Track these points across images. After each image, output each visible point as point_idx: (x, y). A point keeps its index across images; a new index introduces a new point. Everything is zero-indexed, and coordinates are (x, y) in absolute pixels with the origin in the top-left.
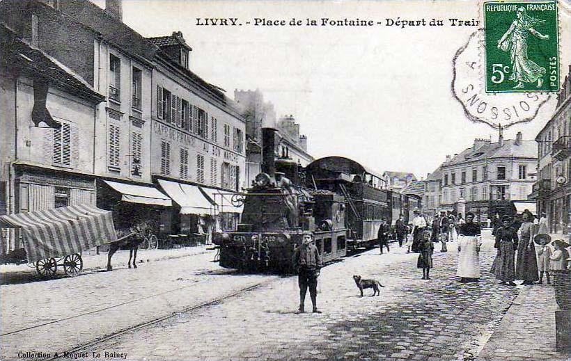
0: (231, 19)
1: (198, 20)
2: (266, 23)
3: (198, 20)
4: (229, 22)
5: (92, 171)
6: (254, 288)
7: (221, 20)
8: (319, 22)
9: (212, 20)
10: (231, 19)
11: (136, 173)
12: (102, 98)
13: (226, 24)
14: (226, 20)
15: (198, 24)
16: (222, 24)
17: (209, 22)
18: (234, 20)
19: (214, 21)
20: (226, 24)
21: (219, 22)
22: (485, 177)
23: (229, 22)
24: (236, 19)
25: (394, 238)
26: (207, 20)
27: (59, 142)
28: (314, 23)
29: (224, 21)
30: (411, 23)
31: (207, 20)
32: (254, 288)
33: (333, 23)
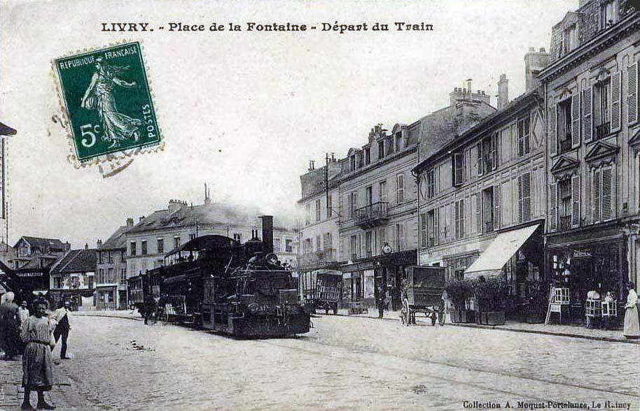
0: (141, 24)
1: (104, 25)
2: (182, 28)
3: (104, 25)
8: (244, 27)
9: (119, 25)
13: (136, 30)
14: (135, 25)
15: (104, 30)
17: (117, 28)
18: (144, 25)
19: (122, 26)
21: (127, 27)
23: (139, 28)
24: (147, 24)
28: (238, 28)
31: (114, 25)
33: (260, 28)
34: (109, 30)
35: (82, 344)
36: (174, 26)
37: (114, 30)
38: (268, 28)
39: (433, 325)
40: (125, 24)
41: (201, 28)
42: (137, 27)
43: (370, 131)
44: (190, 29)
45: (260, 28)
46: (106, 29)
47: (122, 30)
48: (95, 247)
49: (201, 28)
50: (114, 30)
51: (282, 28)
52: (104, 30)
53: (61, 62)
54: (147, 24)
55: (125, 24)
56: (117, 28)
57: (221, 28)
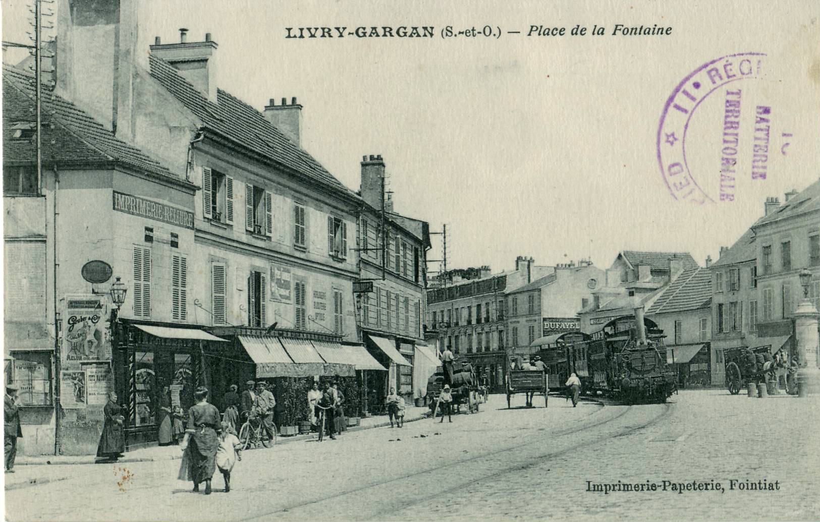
0: (338, 29)
1: (289, 30)
3: (289, 30)
4: (335, 33)
5: (440, 263)
6: (629, 431)
7: (323, 29)
9: (309, 29)
10: (338, 29)
11: (90, 394)
12: (199, 189)
13: (330, 36)
14: (330, 30)
15: (289, 36)
16: (323, 36)
17: (306, 33)
18: (341, 30)
19: (313, 31)
20: (330, 36)
21: (320, 32)
22: (787, 263)
23: (335, 33)
24: (344, 28)
25: (812, 302)
26: (301, 30)
27: (139, 282)
28: (602, 32)
29: (326, 30)
30: (387, 31)
31: (301, 30)
32: (629, 431)
34: (295, 37)
35: (26, 411)
36: (534, 28)
37: (302, 36)
38: (634, 31)
39: (575, 406)
40: (316, 29)
41: (561, 32)
42: (332, 33)
43: (765, 201)
44: (394, 32)
45: (626, 32)
46: (292, 35)
47: (313, 36)
48: (109, 323)
49: (561, 32)
50: (302, 36)
51: (647, 32)
52: (289, 36)
53: (456, 413)
54: (344, 28)
55: (316, 29)
56: (306, 33)
57: (583, 32)
